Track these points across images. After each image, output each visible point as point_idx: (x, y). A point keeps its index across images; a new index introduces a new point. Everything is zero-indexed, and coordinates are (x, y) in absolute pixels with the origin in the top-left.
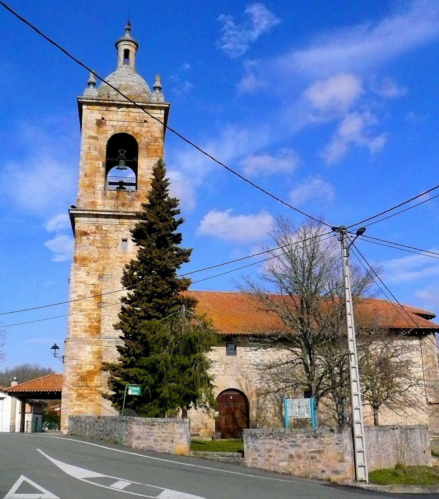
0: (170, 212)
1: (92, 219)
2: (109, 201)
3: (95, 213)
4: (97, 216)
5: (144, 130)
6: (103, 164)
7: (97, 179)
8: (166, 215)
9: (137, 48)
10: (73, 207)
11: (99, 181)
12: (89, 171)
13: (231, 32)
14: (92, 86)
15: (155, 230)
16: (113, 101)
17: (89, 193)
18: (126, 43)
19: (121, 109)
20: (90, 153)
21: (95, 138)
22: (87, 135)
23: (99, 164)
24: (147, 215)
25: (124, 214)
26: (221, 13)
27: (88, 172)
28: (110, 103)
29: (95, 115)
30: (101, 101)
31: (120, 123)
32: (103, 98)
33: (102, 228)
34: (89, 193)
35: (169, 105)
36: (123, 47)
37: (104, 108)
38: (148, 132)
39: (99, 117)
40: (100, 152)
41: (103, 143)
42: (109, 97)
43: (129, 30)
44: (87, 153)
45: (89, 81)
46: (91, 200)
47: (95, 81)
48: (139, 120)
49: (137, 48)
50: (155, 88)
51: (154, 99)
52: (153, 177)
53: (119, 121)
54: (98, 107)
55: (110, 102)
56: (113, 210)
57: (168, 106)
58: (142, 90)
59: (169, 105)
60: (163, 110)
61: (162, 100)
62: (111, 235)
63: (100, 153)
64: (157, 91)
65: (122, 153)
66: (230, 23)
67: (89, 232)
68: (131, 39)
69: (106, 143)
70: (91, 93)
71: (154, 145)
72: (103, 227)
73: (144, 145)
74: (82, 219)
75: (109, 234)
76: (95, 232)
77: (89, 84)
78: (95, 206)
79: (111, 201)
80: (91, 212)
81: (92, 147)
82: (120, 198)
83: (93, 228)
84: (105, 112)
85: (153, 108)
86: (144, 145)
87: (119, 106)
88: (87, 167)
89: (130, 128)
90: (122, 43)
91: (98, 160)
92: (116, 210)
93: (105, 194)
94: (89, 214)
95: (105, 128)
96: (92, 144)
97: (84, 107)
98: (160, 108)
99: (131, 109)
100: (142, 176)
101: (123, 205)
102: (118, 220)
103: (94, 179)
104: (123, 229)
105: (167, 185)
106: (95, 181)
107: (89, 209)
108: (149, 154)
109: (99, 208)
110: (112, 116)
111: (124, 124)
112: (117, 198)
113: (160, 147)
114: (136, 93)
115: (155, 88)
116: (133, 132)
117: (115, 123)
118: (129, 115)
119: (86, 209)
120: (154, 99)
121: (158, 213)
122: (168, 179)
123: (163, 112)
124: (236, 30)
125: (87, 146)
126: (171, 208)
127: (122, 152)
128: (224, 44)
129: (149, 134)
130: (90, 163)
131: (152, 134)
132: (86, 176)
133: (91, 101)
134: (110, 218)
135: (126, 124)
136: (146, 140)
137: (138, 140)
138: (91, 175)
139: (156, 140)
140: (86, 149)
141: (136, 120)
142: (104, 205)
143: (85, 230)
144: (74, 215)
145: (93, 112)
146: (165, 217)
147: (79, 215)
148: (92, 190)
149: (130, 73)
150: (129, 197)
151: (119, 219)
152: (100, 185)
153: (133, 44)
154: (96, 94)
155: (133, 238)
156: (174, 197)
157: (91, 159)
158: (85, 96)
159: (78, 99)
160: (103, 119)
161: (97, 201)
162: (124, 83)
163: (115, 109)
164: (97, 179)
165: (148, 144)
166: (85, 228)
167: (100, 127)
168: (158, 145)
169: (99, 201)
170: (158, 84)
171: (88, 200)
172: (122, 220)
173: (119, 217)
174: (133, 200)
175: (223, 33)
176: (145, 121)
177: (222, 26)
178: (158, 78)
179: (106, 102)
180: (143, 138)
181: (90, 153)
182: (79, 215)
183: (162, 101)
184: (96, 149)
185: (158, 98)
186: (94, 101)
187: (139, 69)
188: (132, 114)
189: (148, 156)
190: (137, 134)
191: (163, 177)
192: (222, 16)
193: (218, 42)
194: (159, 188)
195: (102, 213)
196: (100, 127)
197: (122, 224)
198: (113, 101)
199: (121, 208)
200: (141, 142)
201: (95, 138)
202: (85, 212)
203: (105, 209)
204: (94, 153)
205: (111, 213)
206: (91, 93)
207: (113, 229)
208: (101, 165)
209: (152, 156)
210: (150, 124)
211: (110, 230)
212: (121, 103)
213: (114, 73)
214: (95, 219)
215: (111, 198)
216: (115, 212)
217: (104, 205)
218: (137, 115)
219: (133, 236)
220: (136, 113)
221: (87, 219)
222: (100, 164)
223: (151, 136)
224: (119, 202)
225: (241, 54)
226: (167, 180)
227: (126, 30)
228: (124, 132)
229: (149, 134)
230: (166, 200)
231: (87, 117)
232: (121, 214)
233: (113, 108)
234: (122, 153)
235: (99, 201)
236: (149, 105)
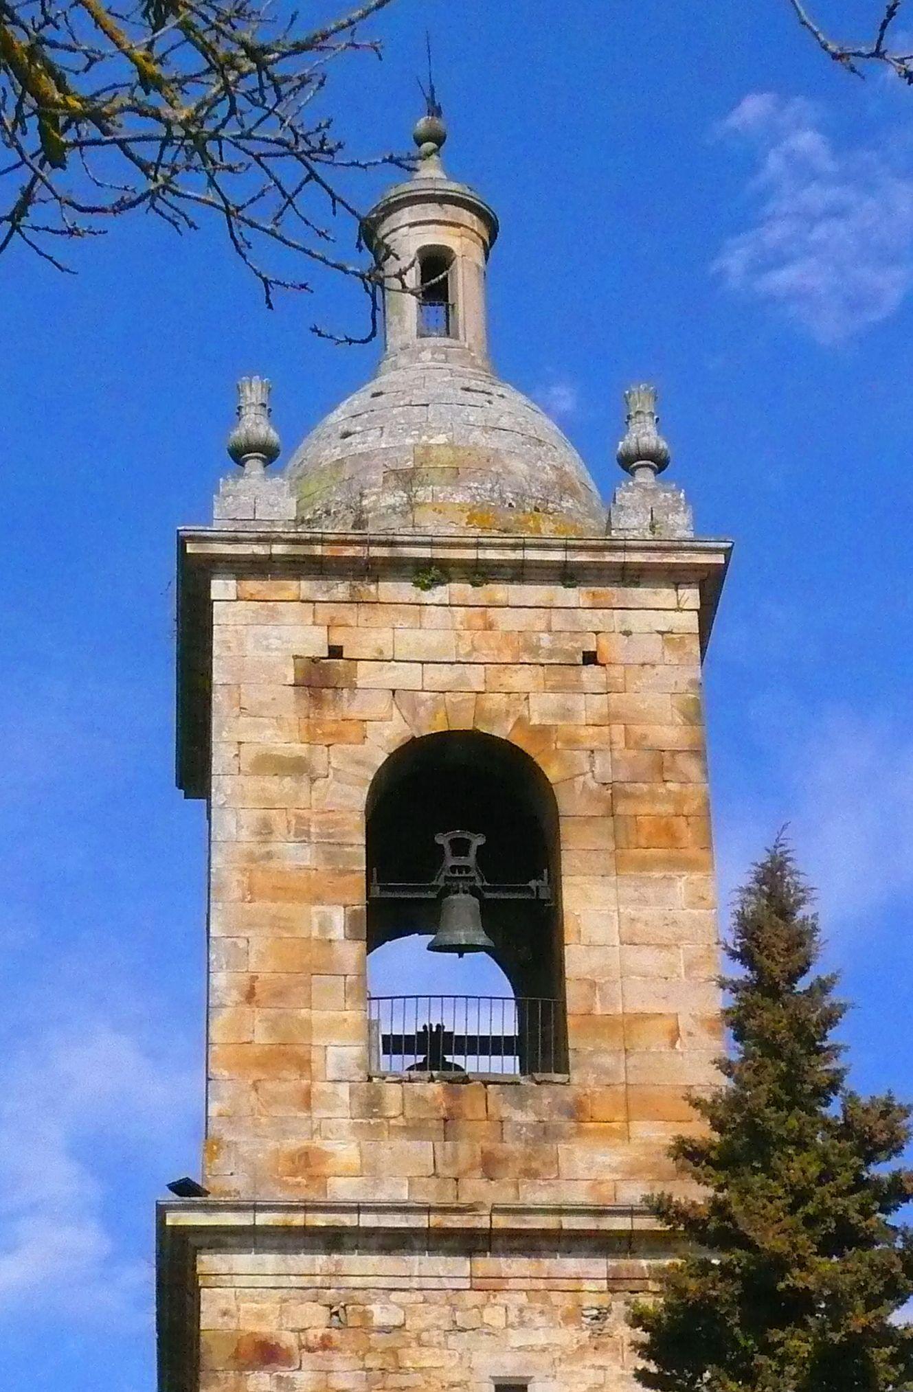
0: (877, 1183)
1: (302, 1261)
2: (402, 1144)
3: (320, 1220)
4: (333, 1240)
5: (588, 707)
6: (352, 920)
7: (317, 1016)
8: (851, 1205)
9: (493, 235)
10: (185, 1188)
11: (331, 1028)
12: (271, 963)
13: (816, 196)
14: (254, 467)
15: (795, 1308)
16: (392, 544)
17: (274, 1100)
18: (432, 211)
19: (440, 593)
20: (269, 856)
21: (298, 768)
22: (249, 753)
23: (325, 926)
24: (736, 1209)
25: (501, 1222)
26: (761, 88)
27: (264, 968)
28: (373, 560)
29: (285, 631)
30: (318, 550)
31: (441, 676)
32: (331, 529)
33: (366, 1316)
34: (274, 1100)
35: (727, 552)
36: (409, 237)
37: (341, 590)
38: (611, 718)
39: (314, 642)
40: (331, 848)
41: (347, 797)
42: (359, 523)
43: (439, 140)
44: (251, 858)
45: (239, 434)
46: (293, 1143)
47: (274, 437)
48: (552, 653)
49: (493, 235)
50: (628, 462)
51: (632, 523)
52: (739, 972)
53: (426, 663)
54: (305, 587)
55: (376, 552)
56: (432, 1201)
57: (720, 559)
58: (551, 476)
59: (727, 552)
60: (689, 584)
61: (680, 524)
62: (428, 1359)
63: (330, 858)
64: (645, 477)
65: (462, 851)
66: (807, 141)
67: (289, 1340)
68: (453, 187)
69: (359, 797)
70: (257, 503)
71: (654, 797)
72: (375, 1308)
73: (594, 798)
74: (243, 1261)
75: (414, 1352)
76: (326, 1344)
77: (239, 455)
78: (317, 1179)
79: (414, 1146)
80: (298, 1219)
81: (279, 820)
82: (467, 1128)
83: (315, 1318)
84: (349, 614)
85: (630, 576)
86: (594, 798)
87: (430, 573)
88: (259, 940)
89: (496, 701)
90: (406, 215)
91: (318, 900)
92: (448, 1199)
93: (372, 1105)
94: (288, 1230)
95: (354, 708)
96: (288, 805)
97: (221, 588)
98: (675, 577)
99: (501, 591)
100: (593, 985)
101: (490, 1166)
102: (462, 1265)
103: (304, 1012)
104: (494, 1317)
105: (829, 1020)
106: (307, 1026)
107: (282, 1196)
108: (648, 847)
109: (343, 1189)
110: (387, 634)
111: (462, 680)
112: (449, 1124)
113: (691, 806)
114: (521, 495)
115: (628, 462)
116: (521, 722)
117: (407, 676)
118: (489, 626)
119: (263, 1197)
120: (634, 522)
121: (800, 1197)
122: (833, 979)
123: (691, 597)
124: (844, 178)
125: (251, 816)
126: (870, 1159)
127: (460, 847)
128: (781, 260)
129: (618, 730)
130: (276, 921)
131: (638, 729)
132: (250, 996)
133: (260, 550)
134: (412, 1250)
135: (475, 677)
136: (602, 766)
137: (553, 773)
138: (280, 994)
139: (661, 763)
140: (245, 834)
141: (534, 649)
142: (370, 1170)
143: (266, 1329)
144: (193, 1240)
145: (273, 616)
146: (842, 1220)
147: (221, 1239)
148: (291, 1082)
149: (472, 384)
150: (519, 1116)
151: (470, 1253)
152: (340, 1052)
153: (466, 217)
154: (288, 507)
155: (641, 1364)
156: (882, 1095)
157: (281, 891)
158: (220, 525)
159: (182, 543)
160: (335, 652)
161: (327, 1146)
162: (441, 439)
163: (402, 590)
164: (317, 1016)
165: (614, 793)
166: (260, 1316)
167: (317, 700)
168: (679, 800)
169: (344, 1149)
170: (644, 434)
171: (272, 1145)
172: (487, 1264)
173: (472, 1243)
174: (545, 1133)
175: (762, 197)
176: (590, 658)
177: (753, 165)
178: (641, 400)
179: (350, 552)
180: (582, 756)
181: (269, 856)
182: (221, 1239)
183: (680, 534)
184: (302, 834)
185: (651, 514)
186: (278, 549)
187: (514, 359)
188: (507, 620)
189: (620, 864)
190: (543, 732)
191: (803, 971)
192: (754, 108)
193: (734, 261)
194: (784, 1035)
195: (368, 1220)
196: (317, 700)
197: (490, 1286)
198: (392, 544)
199: (476, 1188)
200: (574, 780)
201: (298, 768)
202: (263, 1219)
203: (383, 1196)
204: (296, 856)
205: (421, 1221)
206: (257, 503)
207: (433, 1316)
208: (338, 931)
209: (644, 865)
210: (616, 671)
211: (414, 1323)
212: (442, 554)
213: (373, 387)
214: (321, 1261)
215: (414, 1130)
216: (444, 1210)
217: (370, 1163)
218: (536, 620)
219: (646, 1351)
220: (524, 609)
221: (271, 1261)
222: (335, 920)
223: (634, 742)
224: (466, 1151)
225: (875, 316)
226: (823, 986)
227: (419, 141)
228: (464, 723)
229: (618, 730)
230: (833, 1110)
231: (241, 645)
232: (483, 1223)
233: (388, 589)
234: (462, 851)
235: (344, 1149)
236: (609, 557)
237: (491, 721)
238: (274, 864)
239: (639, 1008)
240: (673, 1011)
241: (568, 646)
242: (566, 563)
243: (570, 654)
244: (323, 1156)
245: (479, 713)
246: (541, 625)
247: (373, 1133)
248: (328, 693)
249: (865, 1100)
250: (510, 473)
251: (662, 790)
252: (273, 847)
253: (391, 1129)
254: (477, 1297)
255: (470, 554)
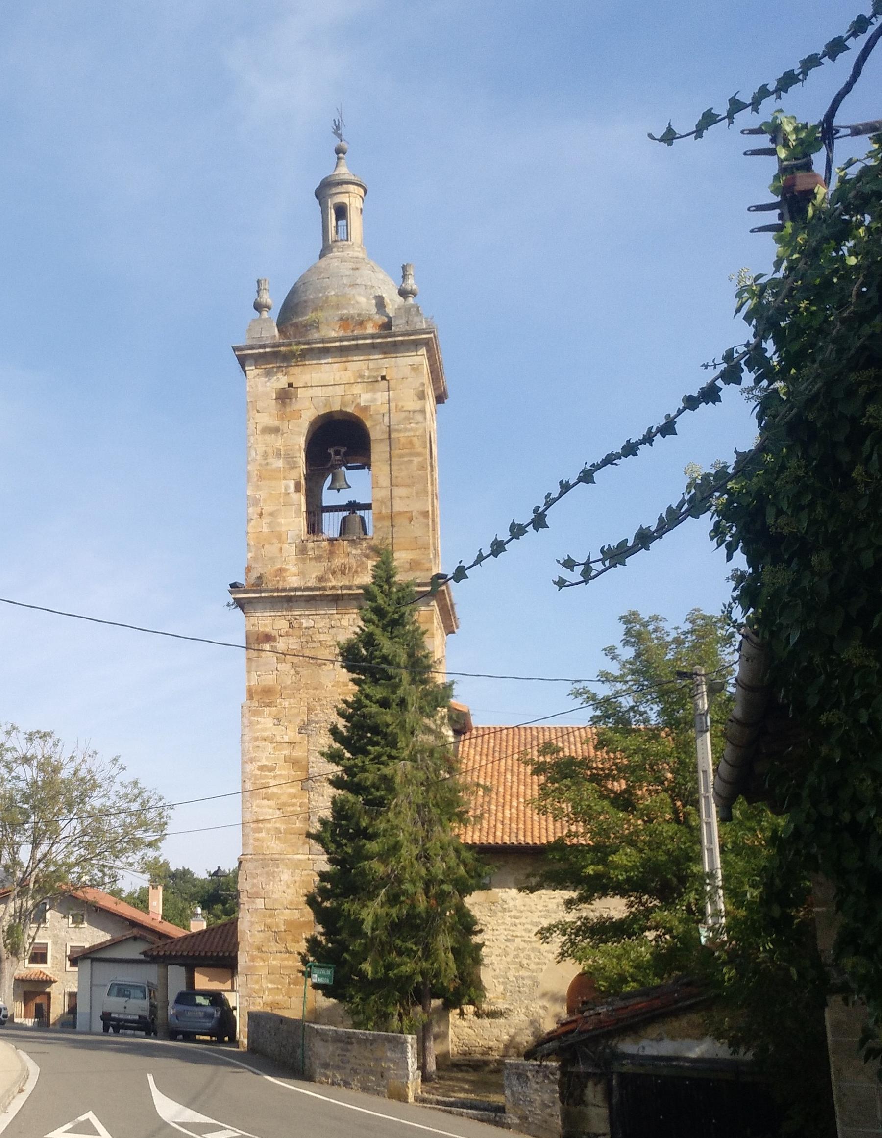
21: (276, 430)
22: (259, 427)
67: (274, 633)
69: (302, 441)
71: (406, 430)
109: (294, 581)
133: (261, 351)
140: (258, 457)
143: (268, 630)
150: (354, 552)
166: (265, 625)
167: (284, 404)
181: (267, 464)
186: (268, 350)
190: (366, 408)
196: (284, 404)
201: (276, 430)
220: (358, 364)
231: (257, 386)
237: (346, 406)
238: (269, 467)
239: (401, 510)
240: (410, 510)
241: (375, 374)
242: (373, 343)
243: (376, 377)
244: (286, 570)
245: (343, 404)
246: (365, 367)
247: (303, 561)
248: (288, 401)
249: (675, 623)
250: (358, 303)
251: (408, 426)
252: (268, 461)
253: (311, 559)
254: (339, 616)
255: (337, 344)
